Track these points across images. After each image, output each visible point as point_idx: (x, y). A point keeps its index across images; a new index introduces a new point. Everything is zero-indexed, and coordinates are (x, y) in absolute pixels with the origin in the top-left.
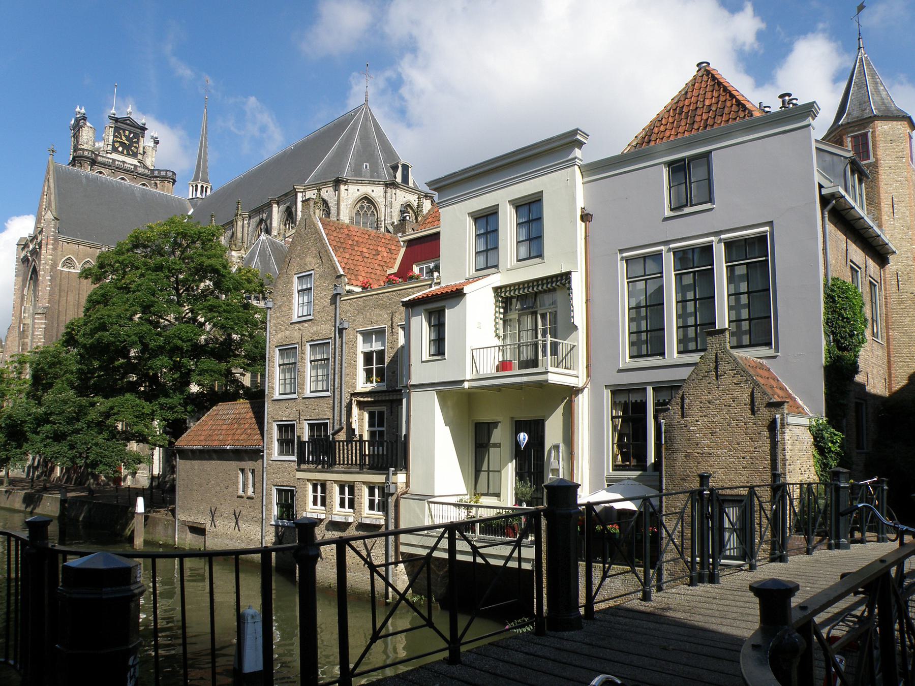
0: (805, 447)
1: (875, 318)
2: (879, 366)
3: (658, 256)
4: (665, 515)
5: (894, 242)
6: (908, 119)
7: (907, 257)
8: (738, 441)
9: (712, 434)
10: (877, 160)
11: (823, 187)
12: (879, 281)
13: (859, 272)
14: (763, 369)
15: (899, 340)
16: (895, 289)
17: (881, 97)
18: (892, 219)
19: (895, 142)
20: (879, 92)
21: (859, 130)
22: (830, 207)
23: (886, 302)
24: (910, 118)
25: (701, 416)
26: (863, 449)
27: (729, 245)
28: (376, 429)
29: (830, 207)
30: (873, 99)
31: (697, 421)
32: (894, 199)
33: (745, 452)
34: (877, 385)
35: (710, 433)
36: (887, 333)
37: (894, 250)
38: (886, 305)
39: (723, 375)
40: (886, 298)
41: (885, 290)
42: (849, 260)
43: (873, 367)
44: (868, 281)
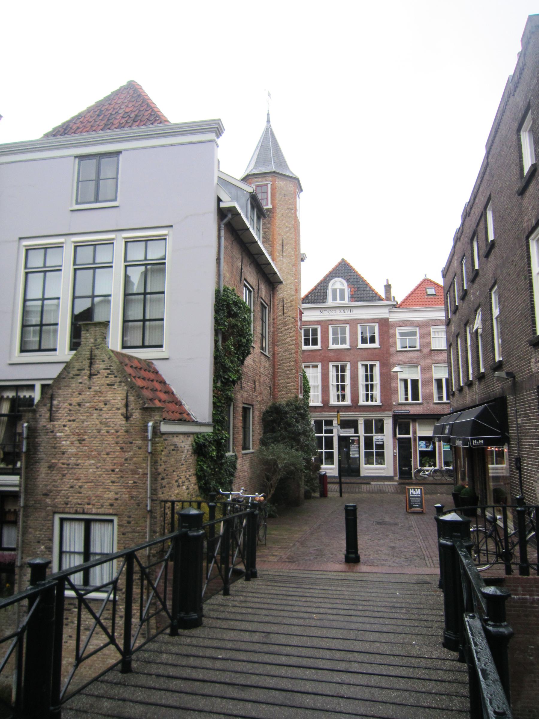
0: (184, 456)
1: (264, 335)
2: (266, 375)
6: (297, 182)
8: (108, 450)
9: (81, 441)
10: (274, 208)
13: (253, 292)
14: (149, 371)
15: (282, 355)
16: (280, 313)
22: (225, 221)
23: (274, 323)
24: (298, 180)
25: (70, 421)
26: (249, 449)
28: (340, 383)
29: (225, 221)
31: (64, 426)
32: (285, 241)
34: (264, 392)
35: (78, 440)
36: (274, 348)
38: (273, 325)
39: (96, 375)
40: (274, 319)
41: (274, 313)
42: (243, 279)
43: (260, 376)
44: (259, 303)
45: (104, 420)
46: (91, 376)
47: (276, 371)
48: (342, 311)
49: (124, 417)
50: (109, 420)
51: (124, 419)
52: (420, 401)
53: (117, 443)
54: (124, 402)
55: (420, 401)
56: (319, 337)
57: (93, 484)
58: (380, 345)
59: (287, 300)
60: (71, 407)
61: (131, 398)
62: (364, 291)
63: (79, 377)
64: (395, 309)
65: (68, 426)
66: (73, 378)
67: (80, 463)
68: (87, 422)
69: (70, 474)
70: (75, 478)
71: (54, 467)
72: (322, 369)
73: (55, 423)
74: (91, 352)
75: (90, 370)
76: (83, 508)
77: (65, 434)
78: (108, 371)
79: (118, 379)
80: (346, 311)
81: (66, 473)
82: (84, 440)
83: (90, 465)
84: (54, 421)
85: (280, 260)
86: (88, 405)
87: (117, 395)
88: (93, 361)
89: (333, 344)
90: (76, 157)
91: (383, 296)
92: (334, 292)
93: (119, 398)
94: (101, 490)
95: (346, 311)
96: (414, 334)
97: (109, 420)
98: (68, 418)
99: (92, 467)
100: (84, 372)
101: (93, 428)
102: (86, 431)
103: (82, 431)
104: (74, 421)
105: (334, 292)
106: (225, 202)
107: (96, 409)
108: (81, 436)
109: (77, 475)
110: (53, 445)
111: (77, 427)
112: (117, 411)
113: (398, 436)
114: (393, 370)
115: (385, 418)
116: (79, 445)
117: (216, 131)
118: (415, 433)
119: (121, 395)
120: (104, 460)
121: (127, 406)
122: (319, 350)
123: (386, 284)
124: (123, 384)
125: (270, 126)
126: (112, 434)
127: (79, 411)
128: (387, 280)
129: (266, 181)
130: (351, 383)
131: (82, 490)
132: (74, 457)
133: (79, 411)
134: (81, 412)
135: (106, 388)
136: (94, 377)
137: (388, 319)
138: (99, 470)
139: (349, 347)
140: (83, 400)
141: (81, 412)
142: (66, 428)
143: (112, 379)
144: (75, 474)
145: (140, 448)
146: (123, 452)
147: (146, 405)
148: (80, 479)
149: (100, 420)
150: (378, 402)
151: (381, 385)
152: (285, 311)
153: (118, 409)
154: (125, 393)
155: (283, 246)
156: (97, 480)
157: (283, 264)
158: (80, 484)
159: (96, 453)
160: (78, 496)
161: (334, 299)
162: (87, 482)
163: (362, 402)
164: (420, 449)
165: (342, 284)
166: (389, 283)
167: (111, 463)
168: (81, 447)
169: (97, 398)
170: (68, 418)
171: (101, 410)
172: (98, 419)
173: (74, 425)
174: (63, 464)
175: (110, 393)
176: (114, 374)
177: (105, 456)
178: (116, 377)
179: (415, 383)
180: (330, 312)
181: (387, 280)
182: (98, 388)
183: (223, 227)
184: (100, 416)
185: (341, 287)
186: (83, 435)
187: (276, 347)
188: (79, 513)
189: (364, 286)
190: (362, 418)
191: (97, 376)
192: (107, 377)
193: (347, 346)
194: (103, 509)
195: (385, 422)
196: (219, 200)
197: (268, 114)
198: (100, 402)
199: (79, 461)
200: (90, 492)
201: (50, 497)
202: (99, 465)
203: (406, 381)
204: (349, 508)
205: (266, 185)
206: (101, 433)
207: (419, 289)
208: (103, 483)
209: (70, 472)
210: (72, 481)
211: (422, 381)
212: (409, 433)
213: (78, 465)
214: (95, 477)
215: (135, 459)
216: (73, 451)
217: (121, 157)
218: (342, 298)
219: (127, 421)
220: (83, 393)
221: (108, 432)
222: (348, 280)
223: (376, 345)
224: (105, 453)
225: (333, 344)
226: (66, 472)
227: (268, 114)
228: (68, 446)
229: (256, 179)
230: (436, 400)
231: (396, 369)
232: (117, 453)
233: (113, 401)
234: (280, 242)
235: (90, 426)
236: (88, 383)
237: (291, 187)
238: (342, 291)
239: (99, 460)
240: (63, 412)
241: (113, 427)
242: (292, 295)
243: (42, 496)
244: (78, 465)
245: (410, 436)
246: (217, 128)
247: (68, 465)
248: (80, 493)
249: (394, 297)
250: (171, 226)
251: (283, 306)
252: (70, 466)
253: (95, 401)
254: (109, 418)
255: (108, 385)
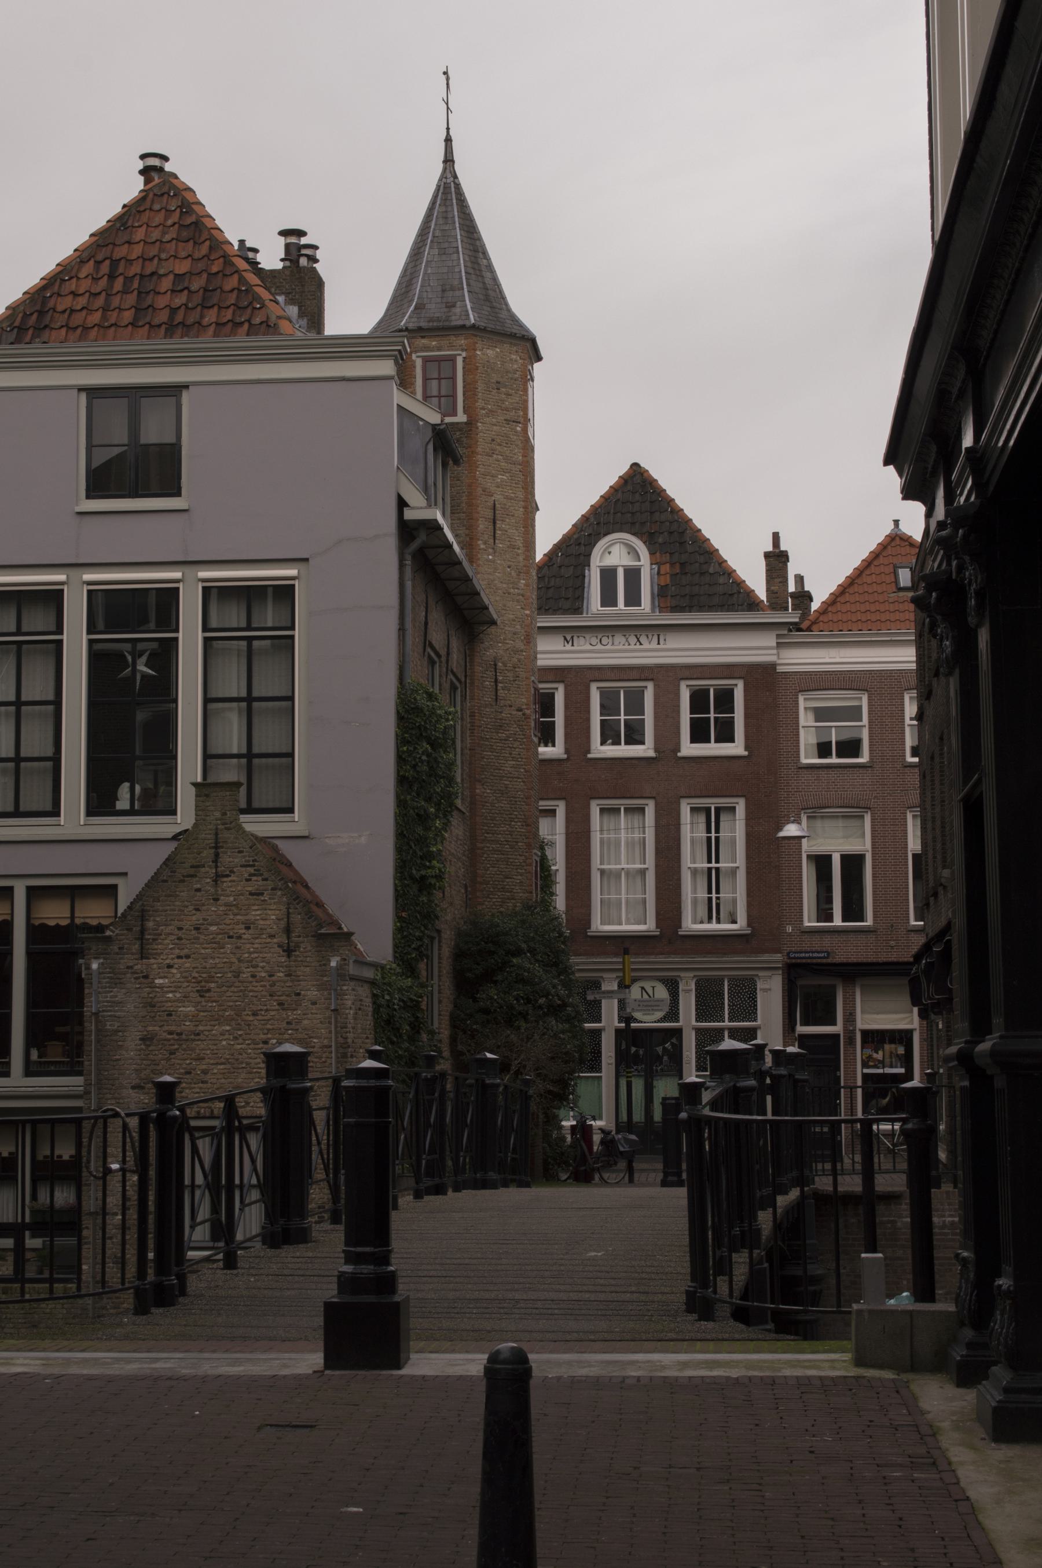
3: (53, 598)
4: (843, 1087)
5: (487, 591)
6: (528, 345)
7: (515, 634)
8: (254, 1008)
9: (202, 993)
10: (470, 423)
11: (407, 505)
12: (463, 680)
17: (484, 283)
18: (491, 550)
19: (505, 386)
20: (480, 270)
21: (439, 350)
22: (415, 545)
25: (179, 957)
27: (212, 593)
29: (415, 545)
30: (468, 285)
31: (170, 966)
33: (269, 1030)
35: (198, 991)
37: (495, 616)
39: (227, 876)
40: (472, 715)
45: (246, 955)
46: (218, 878)
47: (479, 845)
48: (633, 640)
49: (284, 951)
50: (256, 955)
51: (285, 954)
52: (869, 922)
53: (271, 995)
54: (283, 924)
55: (869, 922)
56: (559, 718)
57: (228, 1066)
58: (747, 748)
59: (505, 665)
60: (180, 933)
61: (296, 918)
62: (702, 574)
63: (195, 879)
64: (797, 637)
65: (176, 966)
66: (183, 881)
67: (203, 1031)
68: (213, 958)
69: (184, 1050)
70: (193, 1056)
71: (152, 1039)
72: (568, 821)
73: (152, 961)
74: (216, 834)
75: (217, 867)
76: (210, 1108)
77: (172, 980)
78: (251, 870)
79: (270, 884)
80: (643, 639)
81: (177, 1049)
82: (209, 991)
83: (222, 1034)
84: (149, 958)
85: (488, 560)
86: (214, 928)
87: (269, 912)
88: (220, 850)
89: (603, 743)
90: (81, 389)
91: (762, 593)
92: (608, 575)
93: (273, 917)
94: (243, 1075)
95: (643, 639)
96: (854, 713)
97: (256, 955)
98: (177, 951)
99: (226, 1036)
100: (203, 870)
101: (225, 970)
102: (213, 974)
103: (204, 975)
104: (188, 957)
105: (608, 575)
106: (413, 508)
107: (230, 937)
108: (203, 984)
109: (197, 1051)
110: (149, 1000)
111: (194, 968)
112: (269, 940)
113: (801, 1029)
114: (781, 834)
115: (761, 974)
116: (199, 999)
117: (395, 356)
118: (850, 1018)
119: (278, 912)
120: (249, 1025)
121: (288, 931)
122: (559, 761)
123: (770, 548)
124: (279, 893)
125: (455, 177)
126: (262, 979)
127: (198, 938)
128: (776, 537)
129: (451, 347)
130: (657, 866)
131: (208, 1076)
132: (191, 1021)
133: (198, 938)
134: (201, 941)
135: (248, 899)
136: (225, 879)
137: (773, 666)
138: (240, 1041)
139: (651, 753)
140: (204, 919)
141: (201, 941)
142: (174, 971)
143: (257, 883)
144: (193, 1050)
145: (314, 1003)
146: (283, 1009)
147: (323, 931)
148: (204, 1059)
149: (238, 956)
150: (741, 925)
151: (749, 873)
152: (501, 692)
153: (272, 936)
154: (283, 908)
155: (494, 523)
156: (237, 1060)
157: (496, 569)
158: (204, 1067)
159: (232, 1013)
160: (201, 1088)
161: (608, 598)
162: (217, 1064)
163: (691, 924)
164: (866, 1071)
165: (633, 552)
166: (783, 548)
167: (262, 1029)
168: (204, 1004)
169: (232, 917)
170: (177, 951)
171: (240, 937)
172: (234, 954)
173: (188, 964)
174: (171, 1033)
175: (256, 907)
176: (261, 875)
177: (251, 1018)
178: (266, 880)
179: (853, 863)
180: (594, 641)
181: (776, 537)
182: (232, 899)
183: (409, 557)
184: (238, 948)
185: (630, 562)
186: (207, 982)
187: (478, 786)
188: (204, 1118)
189: (702, 559)
190: (691, 974)
191: (230, 879)
192: (247, 880)
193: (644, 750)
194: (248, 1109)
195: (760, 985)
196: (402, 504)
197: (448, 140)
198: (237, 923)
199: (201, 1028)
200: (223, 1081)
201: (146, 1090)
202: (240, 1033)
203: (822, 863)
204: (668, 1102)
205: (452, 360)
206: (241, 978)
207: (873, 569)
208: (248, 1064)
209: (184, 1046)
210: (188, 1062)
211: (874, 859)
212: (834, 1023)
213: (198, 1034)
214: (232, 1055)
215: (305, 1022)
216: (189, 1009)
217: (185, 396)
218: (633, 598)
219: (289, 956)
220: (204, 908)
221: (253, 976)
222: (650, 540)
223: (736, 748)
224: (250, 1013)
225: (603, 743)
226: (176, 1047)
227: (448, 140)
228: (178, 1000)
229: (424, 341)
230: (809, 922)
231: (791, 830)
232: (273, 1013)
233: (262, 922)
234: (489, 514)
235: (219, 966)
236: (212, 890)
237: (515, 357)
238: (633, 575)
239: (239, 1024)
240: (166, 942)
241: (263, 968)
242: (517, 651)
243: (131, 1091)
244: (198, 1034)
245: (837, 1029)
246: (399, 351)
247: (181, 1034)
248: (205, 1082)
249: (800, 579)
250: (306, 560)
251: (496, 681)
252: (184, 1037)
253: (228, 922)
254: (254, 952)
255: (251, 894)
